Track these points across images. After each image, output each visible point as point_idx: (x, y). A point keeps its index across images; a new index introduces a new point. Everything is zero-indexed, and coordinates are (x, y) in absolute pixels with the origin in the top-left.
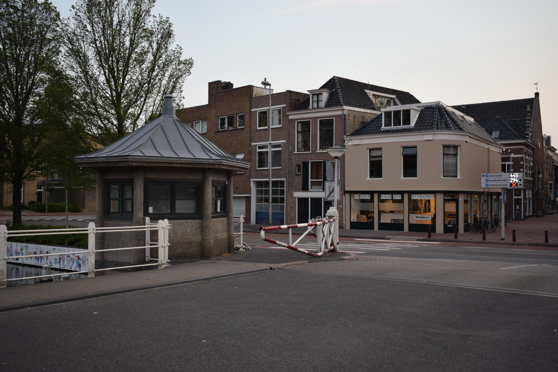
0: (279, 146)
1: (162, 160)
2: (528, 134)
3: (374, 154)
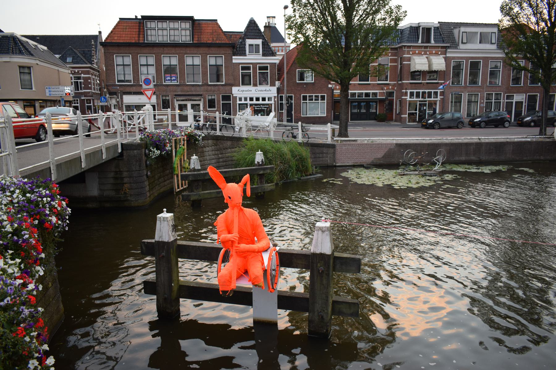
2: (93, 61)
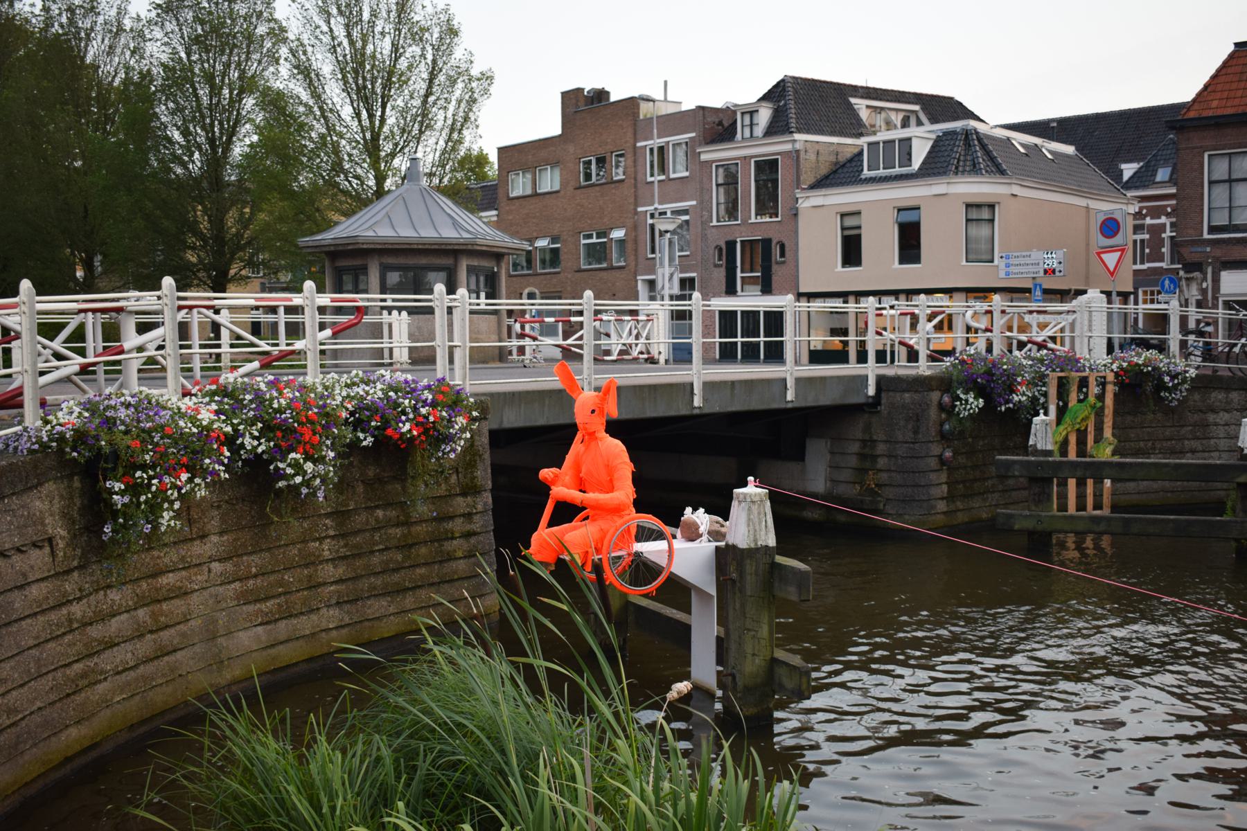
0: (685, 212)
1: (421, 241)
3: (849, 222)
